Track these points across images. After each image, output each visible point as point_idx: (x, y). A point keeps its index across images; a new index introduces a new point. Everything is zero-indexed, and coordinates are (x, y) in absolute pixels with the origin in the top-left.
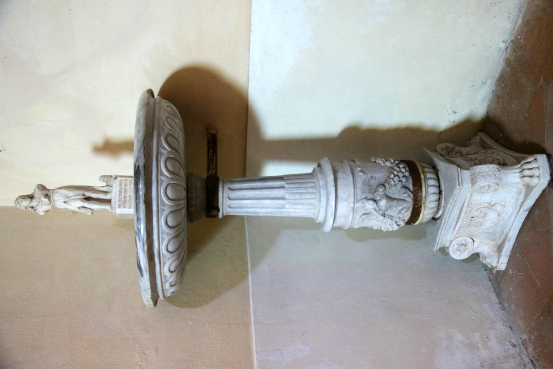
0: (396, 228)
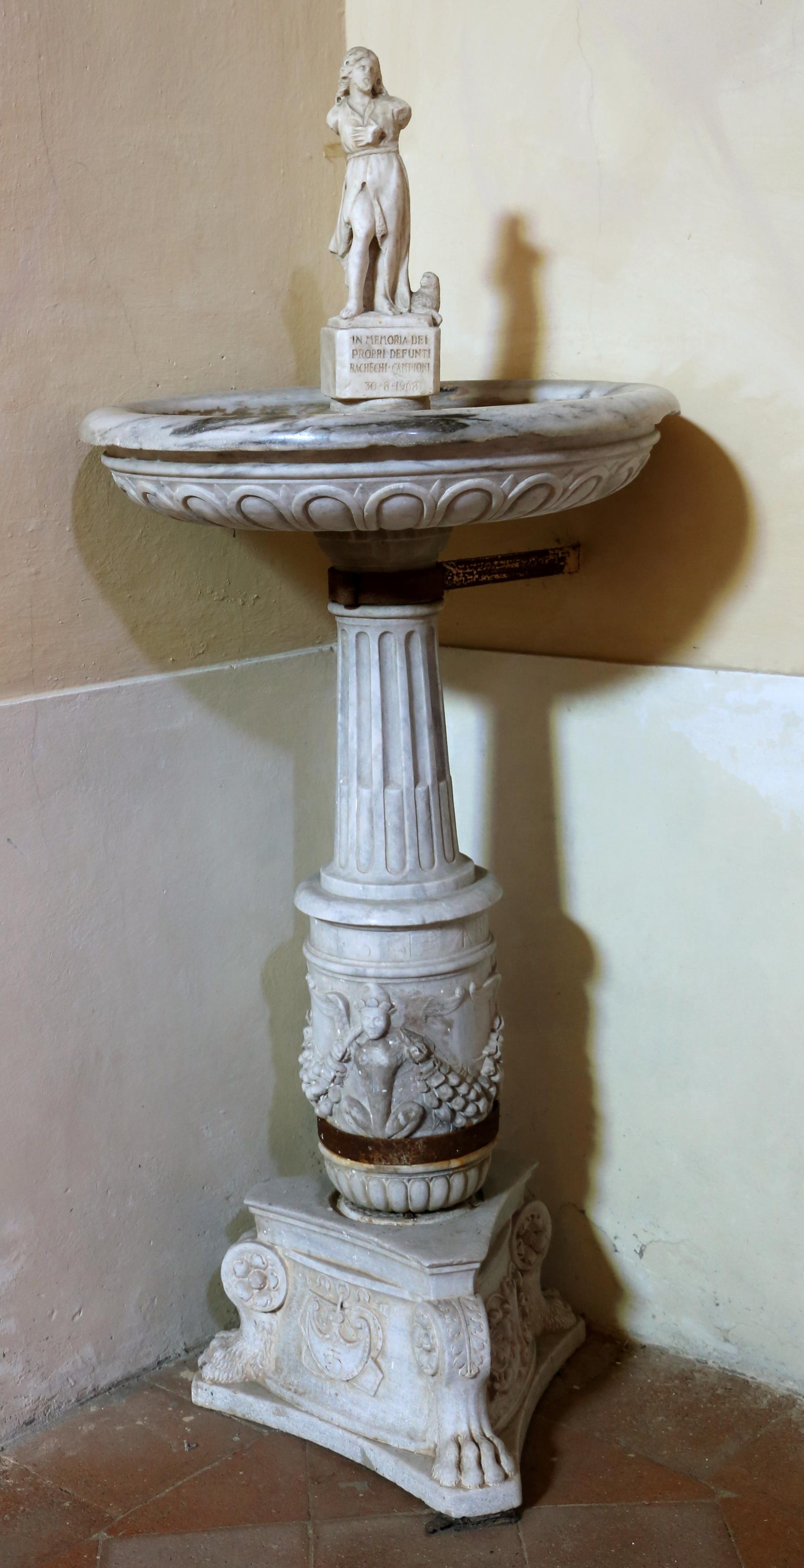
0: (310, 1092)
